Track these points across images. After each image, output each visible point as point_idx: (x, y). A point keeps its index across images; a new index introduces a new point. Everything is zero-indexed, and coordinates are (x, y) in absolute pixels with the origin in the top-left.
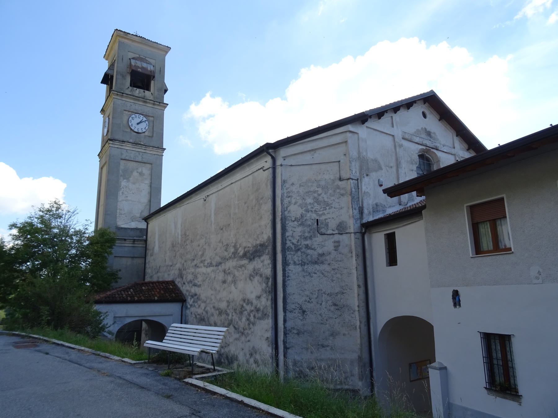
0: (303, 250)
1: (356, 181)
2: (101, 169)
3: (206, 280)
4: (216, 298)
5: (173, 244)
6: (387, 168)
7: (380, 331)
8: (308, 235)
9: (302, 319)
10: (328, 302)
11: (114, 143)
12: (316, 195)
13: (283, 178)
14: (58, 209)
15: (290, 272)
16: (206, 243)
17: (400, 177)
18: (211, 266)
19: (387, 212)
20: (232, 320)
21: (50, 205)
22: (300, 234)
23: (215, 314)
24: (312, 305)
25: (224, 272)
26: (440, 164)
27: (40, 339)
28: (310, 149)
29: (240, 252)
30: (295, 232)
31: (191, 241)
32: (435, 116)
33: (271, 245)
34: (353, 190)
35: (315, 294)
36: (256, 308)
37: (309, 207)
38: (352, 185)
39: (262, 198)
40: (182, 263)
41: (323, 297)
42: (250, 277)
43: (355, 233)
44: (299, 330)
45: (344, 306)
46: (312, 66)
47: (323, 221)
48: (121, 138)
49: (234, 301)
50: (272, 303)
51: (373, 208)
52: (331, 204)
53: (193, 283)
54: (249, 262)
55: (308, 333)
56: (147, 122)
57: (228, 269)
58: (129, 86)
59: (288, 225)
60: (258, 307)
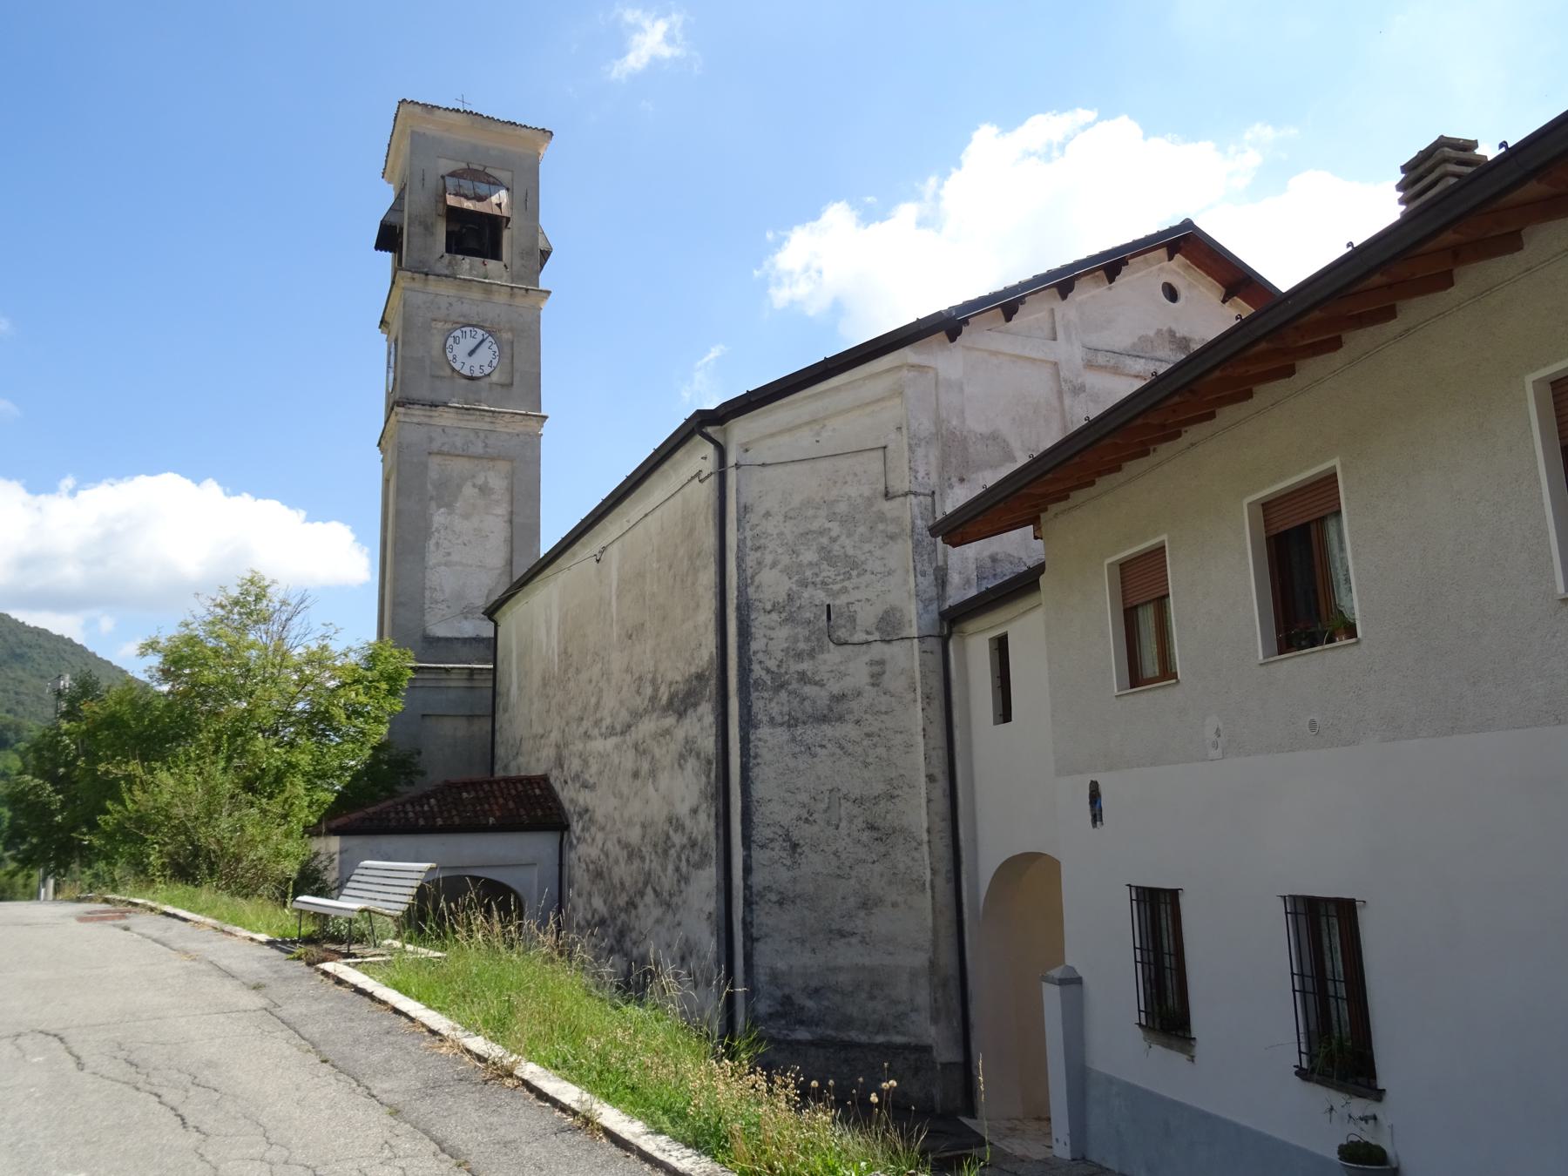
0: (794, 686)
1: (930, 499)
2: (386, 481)
4: (622, 815)
5: (544, 679)
10: (855, 821)
11: (409, 411)
12: (824, 540)
13: (742, 501)
14: (258, 599)
22: (786, 645)
24: (816, 828)
30: (772, 639)
31: (577, 669)
34: (919, 522)
35: (822, 801)
37: (808, 573)
38: (916, 511)
39: (699, 554)
44: (782, 893)
45: (894, 832)
48: (428, 395)
55: (806, 901)
59: (756, 623)
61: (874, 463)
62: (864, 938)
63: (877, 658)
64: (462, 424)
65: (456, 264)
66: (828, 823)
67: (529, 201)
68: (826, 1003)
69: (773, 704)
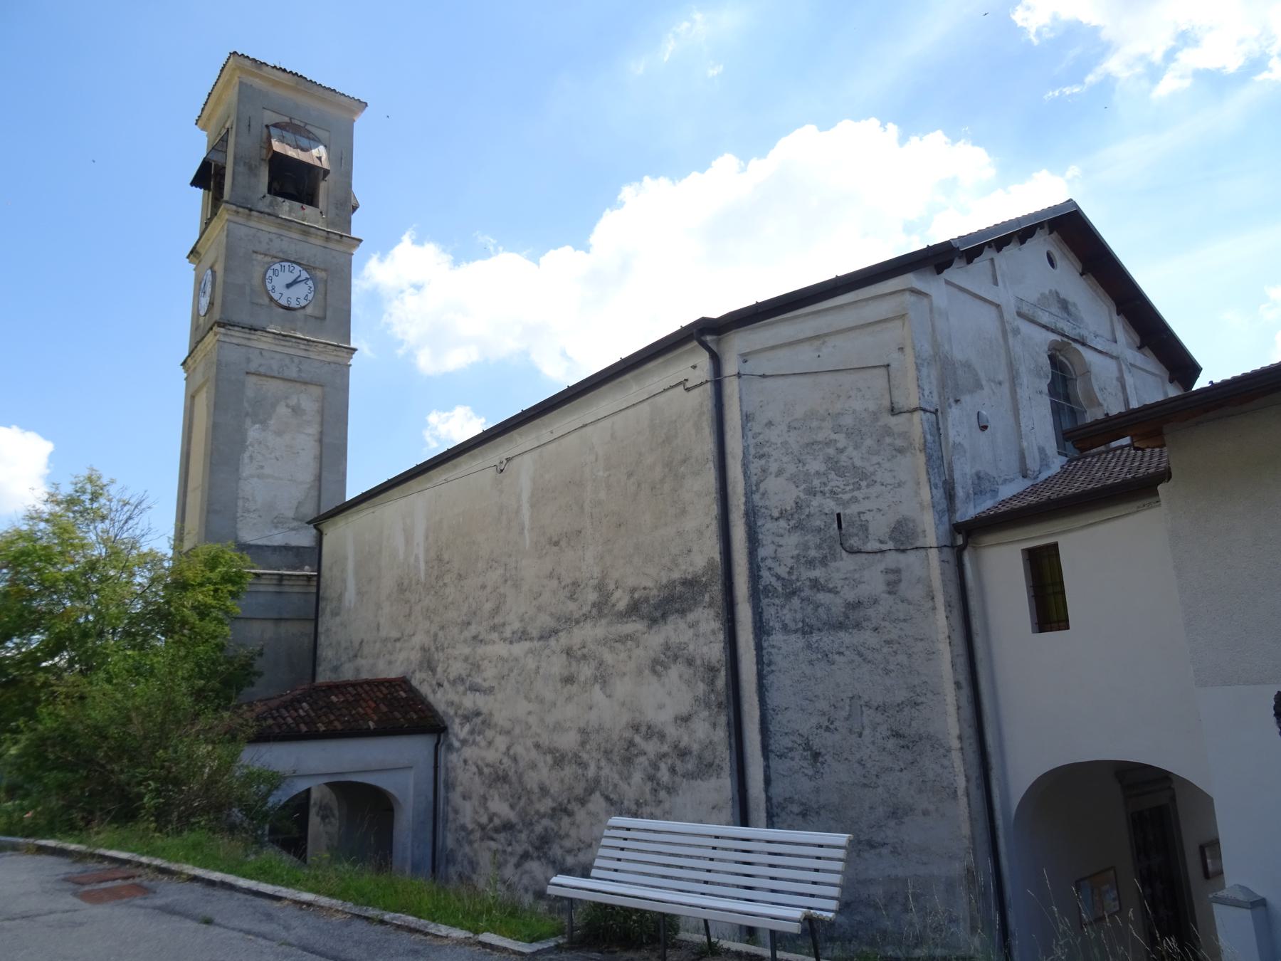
2: (191, 398)
3: (508, 675)
4: (542, 720)
6: (992, 384)
7: (1019, 800)
8: (817, 555)
9: (811, 776)
11: (229, 332)
12: (831, 451)
13: (744, 409)
15: (773, 651)
16: (506, 581)
17: (1020, 406)
18: (526, 640)
19: (999, 494)
20: (597, 781)
21: (73, 487)
22: (795, 552)
23: (542, 764)
24: (837, 737)
25: (568, 654)
26: (1090, 379)
27: (140, 865)
28: (809, 334)
29: (618, 602)
30: (781, 546)
32: (1073, 264)
33: (720, 582)
34: (928, 437)
36: (676, 747)
37: (816, 482)
39: (684, 461)
40: (432, 632)
41: (864, 715)
42: (653, 666)
43: (939, 548)
45: (920, 739)
46: (647, 179)
47: (854, 519)
49: (603, 729)
50: (730, 734)
51: (973, 484)
52: (873, 474)
53: (468, 683)
54: (650, 627)
56: (310, 283)
57: (578, 646)
58: (266, 191)
59: (763, 529)
60: (682, 745)
61: (878, 379)
62: (895, 848)
63: (893, 566)
64: (279, 349)
65: (277, 205)
66: (851, 731)
67: (344, 157)
68: (858, 918)
69: (785, 611)
